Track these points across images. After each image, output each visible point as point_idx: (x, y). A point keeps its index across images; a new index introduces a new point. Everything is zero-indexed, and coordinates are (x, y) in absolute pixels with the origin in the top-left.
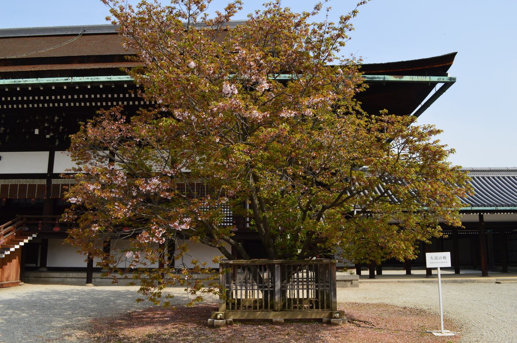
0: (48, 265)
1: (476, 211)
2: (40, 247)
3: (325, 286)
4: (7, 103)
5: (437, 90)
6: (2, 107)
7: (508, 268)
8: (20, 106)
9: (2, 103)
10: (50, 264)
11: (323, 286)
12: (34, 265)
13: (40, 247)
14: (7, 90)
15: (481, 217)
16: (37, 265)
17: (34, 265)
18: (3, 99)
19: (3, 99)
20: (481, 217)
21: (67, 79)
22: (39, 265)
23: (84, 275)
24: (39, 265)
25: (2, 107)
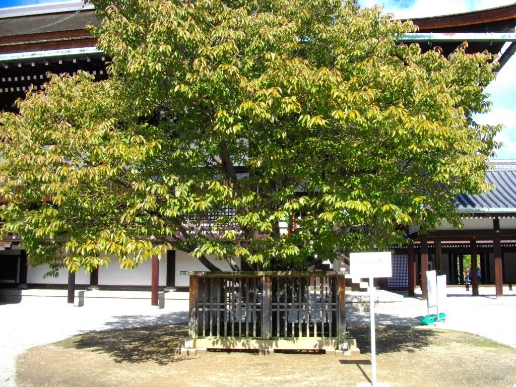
0: (29, 281)
1: (492, 214)
2: (19, 259)
3: (211, 307)
4: (8, 85)
5: (503, 53)
6: (4, 90)
7: (24, 292)
8: (12, 90)
9: (3, 86)
10: (30, 280)
11: (208, 307)
12: (13, 281)
13: (19, 259)
14: (47, 64)
15: (496, 222)
16: (16, 281)
17: (13, 281)
18: (4, 80)
19: (4, 80)
20: (496, 222)
21: (34, 54)
22: (18, 282)
23: (65, 292)
24: (18, 282)
25: (4, 90)
